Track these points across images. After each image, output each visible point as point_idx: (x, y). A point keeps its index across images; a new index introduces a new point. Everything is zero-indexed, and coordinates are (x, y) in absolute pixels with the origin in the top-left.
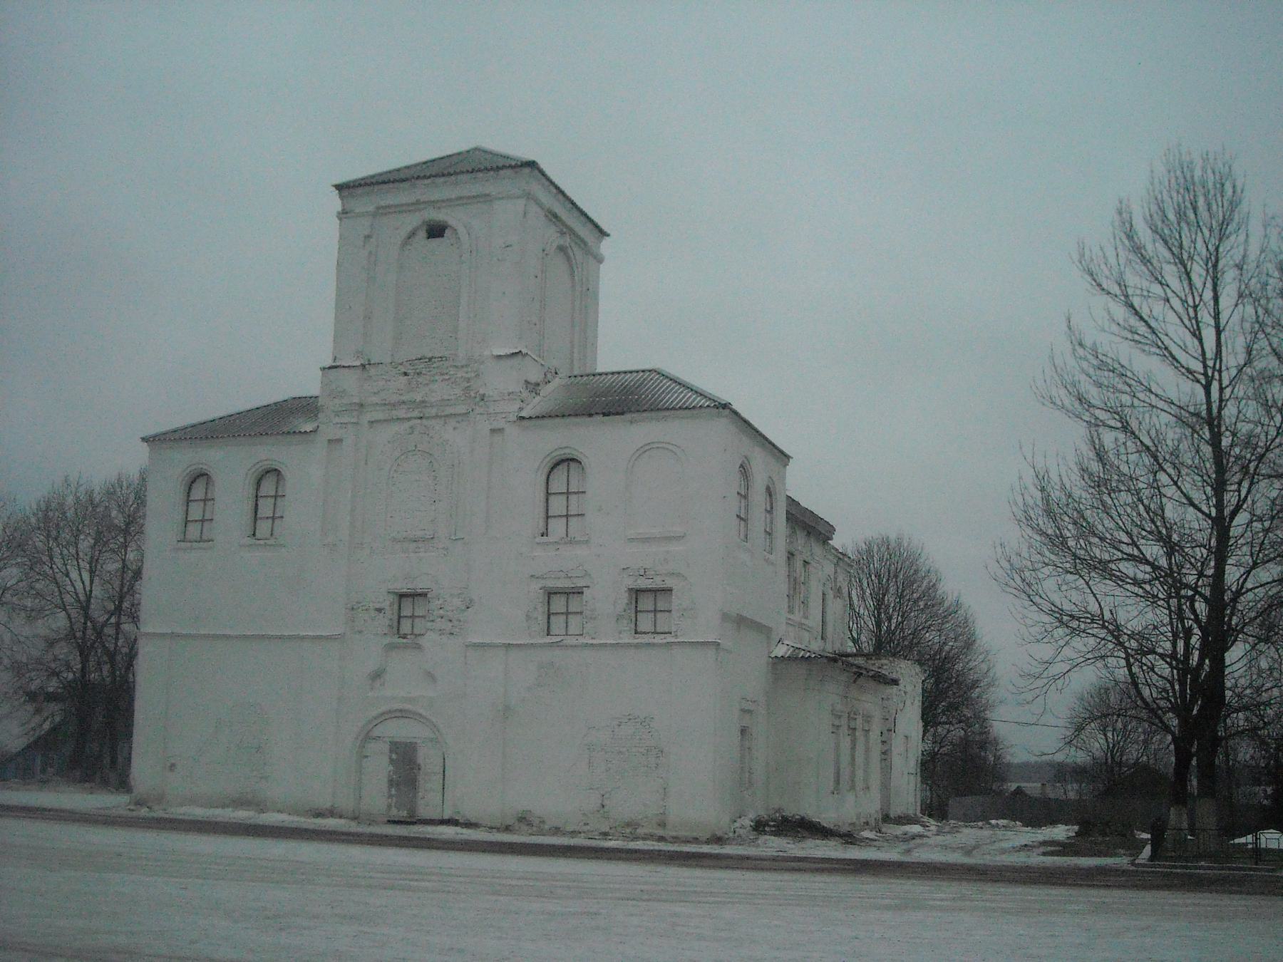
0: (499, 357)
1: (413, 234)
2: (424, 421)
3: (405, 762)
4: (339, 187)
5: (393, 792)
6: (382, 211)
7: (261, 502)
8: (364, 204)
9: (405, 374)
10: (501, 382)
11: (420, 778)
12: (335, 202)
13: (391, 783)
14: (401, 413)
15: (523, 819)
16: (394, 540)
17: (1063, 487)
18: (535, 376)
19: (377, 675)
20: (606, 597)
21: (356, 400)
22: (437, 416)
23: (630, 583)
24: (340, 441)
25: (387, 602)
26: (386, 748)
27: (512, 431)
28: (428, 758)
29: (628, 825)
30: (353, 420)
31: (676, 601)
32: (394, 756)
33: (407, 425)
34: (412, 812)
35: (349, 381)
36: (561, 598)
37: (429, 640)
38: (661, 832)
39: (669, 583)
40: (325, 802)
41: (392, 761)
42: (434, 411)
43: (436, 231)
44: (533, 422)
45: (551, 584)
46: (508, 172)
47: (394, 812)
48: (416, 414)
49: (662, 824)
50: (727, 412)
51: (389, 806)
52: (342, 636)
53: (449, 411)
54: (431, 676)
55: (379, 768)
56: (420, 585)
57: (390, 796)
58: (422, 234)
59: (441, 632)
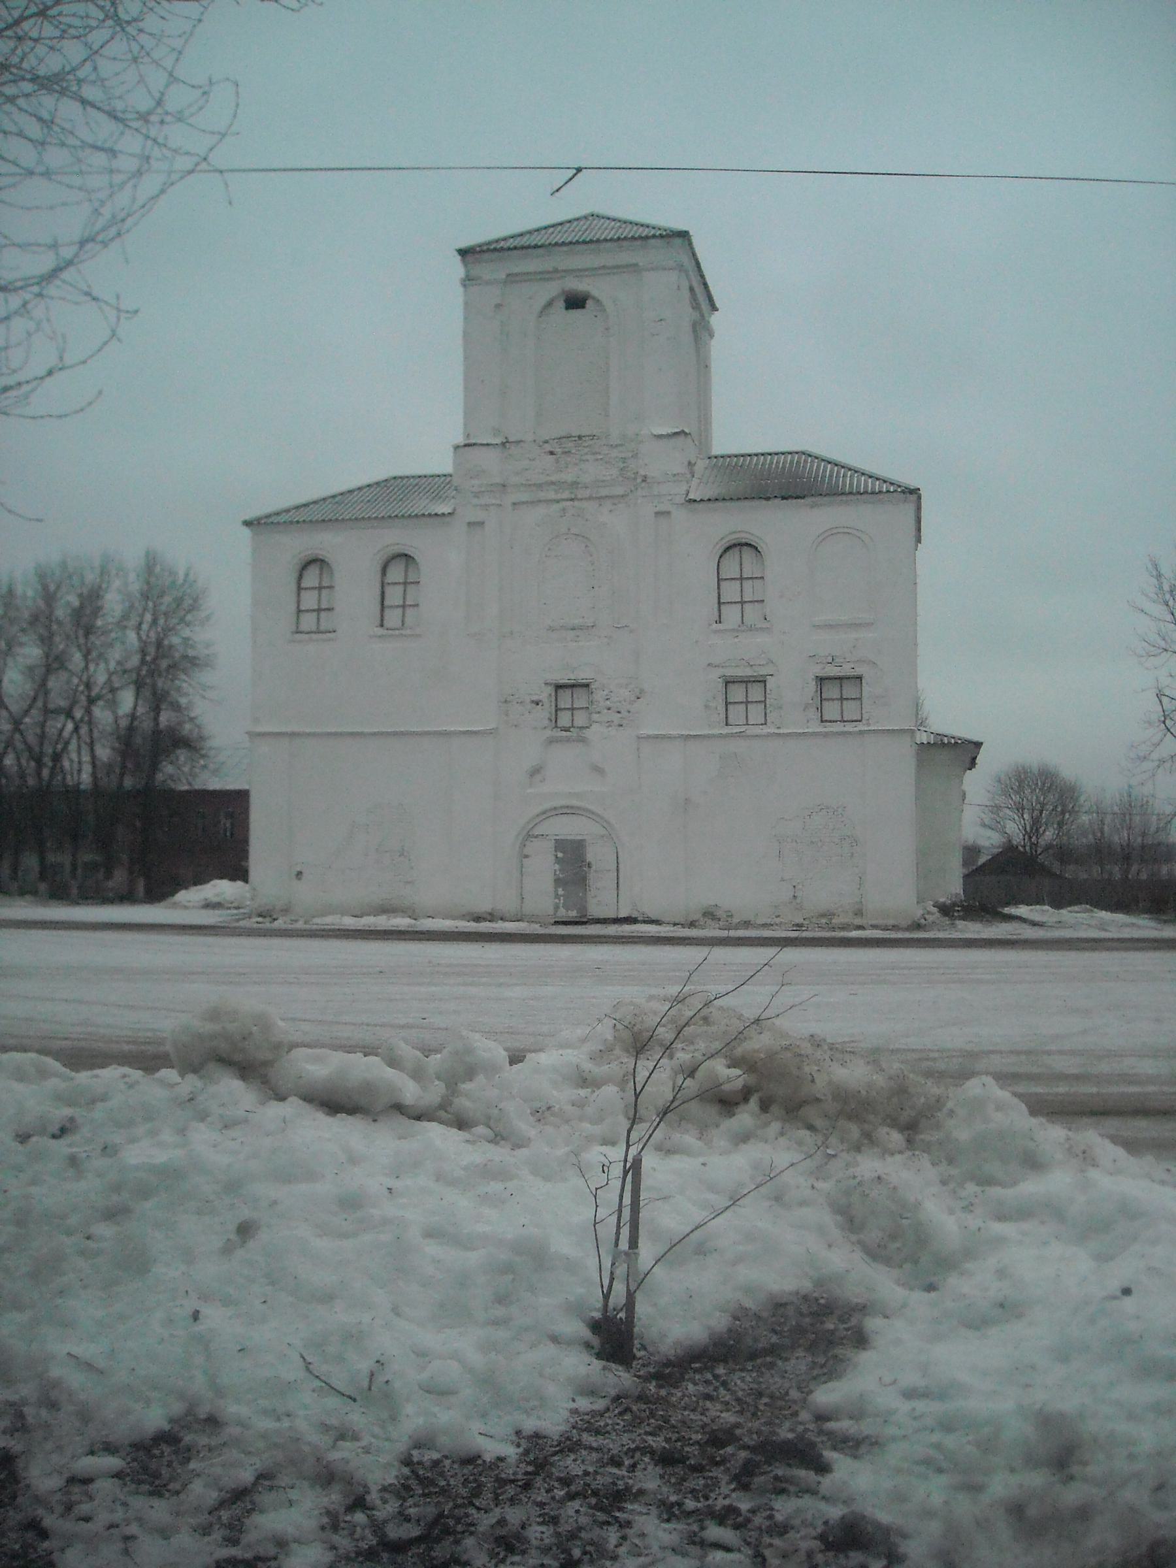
0: (660, 437)
1: (549, 304)
2: (576, 503)
4: (463, 253)
7: (389, 590)
9: (552, 453)
11: (592, 876)
12: (457, 269)
13: (558, 882)
15: (710, 914)
16: (551, 629)
19: (535, 771)
20: (792, 684)
21: (498, 480)
22: (590, 498)
23: (819, 671)
24: (481, 524)
30: (498, 502)
32: (560, 855)
33: (556, 507)
34: (583, 909)
35: (489, 460)
36: (744, 687)
42: (587, 493)
43: (576, 302)
45: (730, 672)
48: (566, 495)
49: (859, 913)
51: (557, 907)
52: (490, 732)
53: (604, 492)
54: (598, 770)
55: (543, 867)
56: (582, 676)
57: (557, 896)
58: (561, 304)
59: (609, 723)
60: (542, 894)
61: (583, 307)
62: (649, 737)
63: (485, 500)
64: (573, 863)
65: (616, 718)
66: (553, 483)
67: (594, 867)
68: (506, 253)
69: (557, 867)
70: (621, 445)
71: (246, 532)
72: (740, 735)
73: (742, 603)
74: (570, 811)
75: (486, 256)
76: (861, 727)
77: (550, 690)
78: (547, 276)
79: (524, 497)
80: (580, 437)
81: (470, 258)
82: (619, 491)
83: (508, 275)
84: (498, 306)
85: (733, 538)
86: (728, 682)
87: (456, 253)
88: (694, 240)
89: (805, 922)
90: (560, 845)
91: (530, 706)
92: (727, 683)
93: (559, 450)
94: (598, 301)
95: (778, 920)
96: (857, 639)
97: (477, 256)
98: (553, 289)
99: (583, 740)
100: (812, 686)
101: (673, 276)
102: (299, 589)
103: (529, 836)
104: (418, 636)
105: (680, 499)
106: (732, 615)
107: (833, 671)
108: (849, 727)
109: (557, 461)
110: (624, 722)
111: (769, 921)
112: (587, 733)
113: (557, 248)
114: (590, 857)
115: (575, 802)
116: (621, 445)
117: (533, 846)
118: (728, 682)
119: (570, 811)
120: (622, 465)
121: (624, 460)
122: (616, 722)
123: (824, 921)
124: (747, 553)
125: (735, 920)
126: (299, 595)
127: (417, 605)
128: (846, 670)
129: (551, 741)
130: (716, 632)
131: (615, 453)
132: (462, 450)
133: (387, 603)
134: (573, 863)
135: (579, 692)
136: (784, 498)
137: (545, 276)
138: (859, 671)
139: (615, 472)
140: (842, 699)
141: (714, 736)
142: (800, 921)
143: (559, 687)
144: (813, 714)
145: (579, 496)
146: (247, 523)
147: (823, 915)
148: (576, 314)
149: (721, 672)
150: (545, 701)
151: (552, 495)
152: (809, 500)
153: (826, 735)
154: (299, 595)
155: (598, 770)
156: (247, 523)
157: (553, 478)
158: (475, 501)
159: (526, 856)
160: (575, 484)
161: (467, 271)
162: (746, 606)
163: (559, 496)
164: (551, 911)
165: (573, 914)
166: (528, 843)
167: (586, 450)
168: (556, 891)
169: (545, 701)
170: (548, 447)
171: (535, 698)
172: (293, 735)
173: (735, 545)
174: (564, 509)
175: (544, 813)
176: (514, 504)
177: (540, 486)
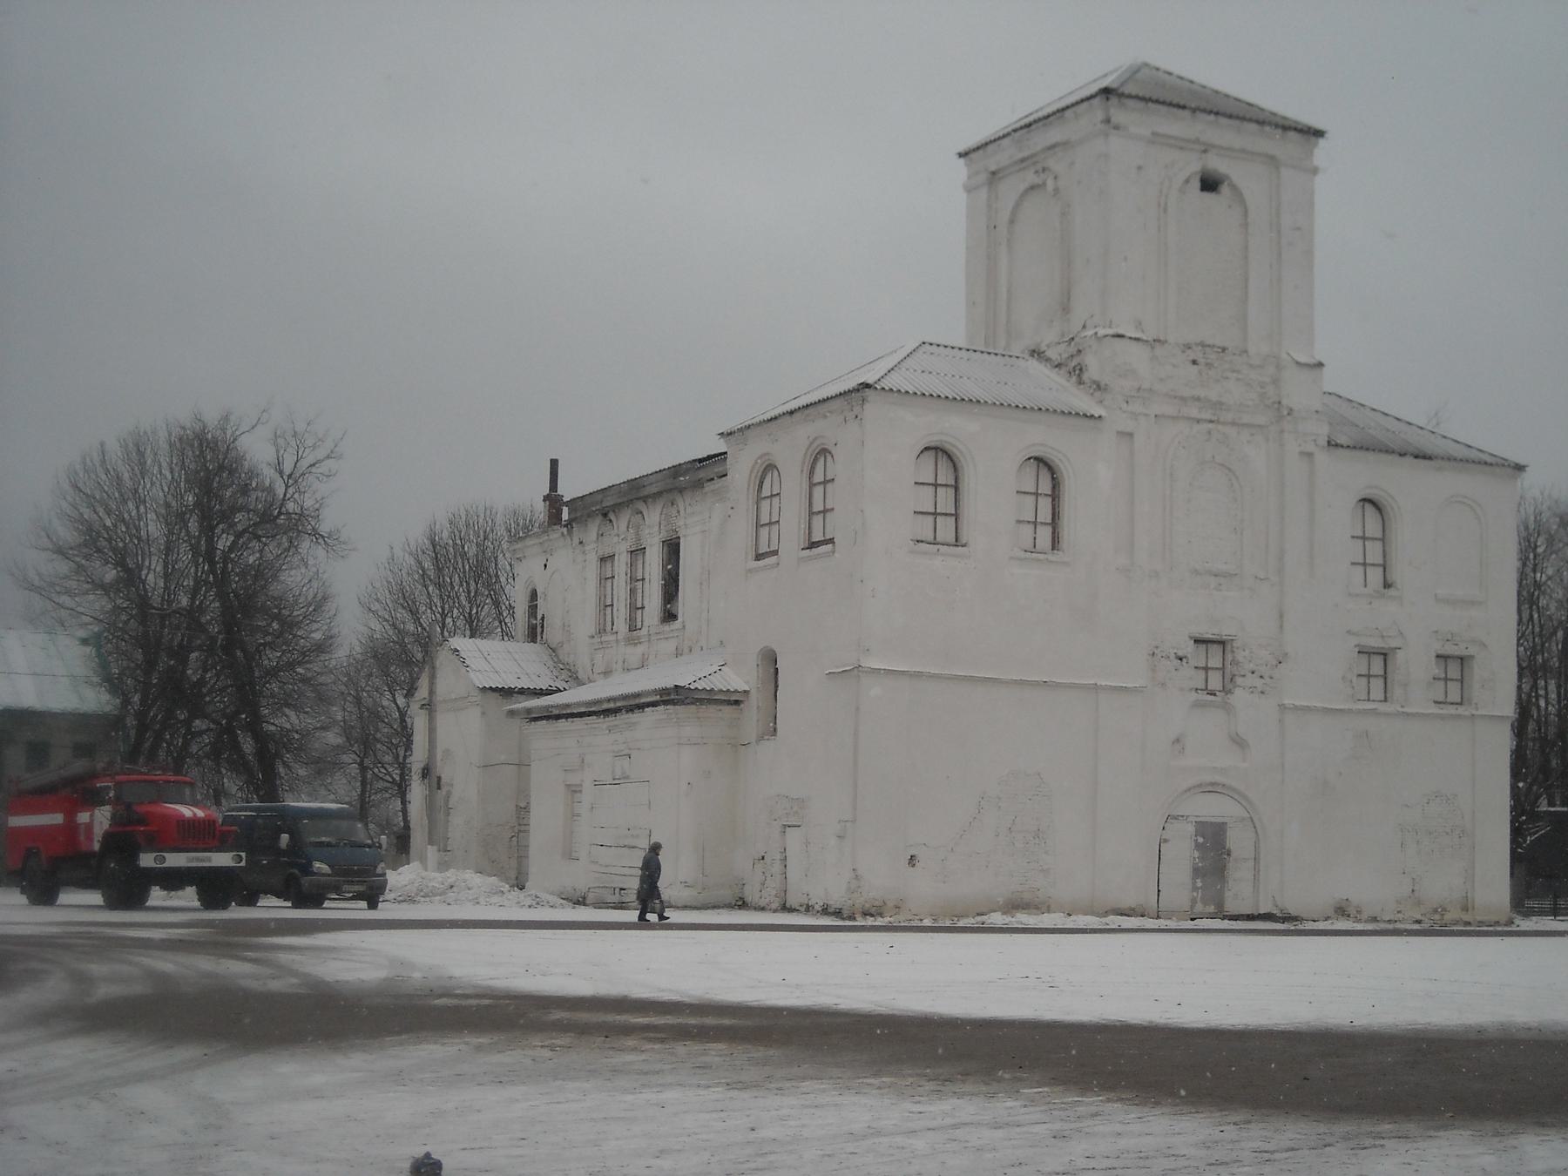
1: (1187, 181)
3: (1213, 840)
5: (1199, 884)
9: (1194, 362)
11: (1231, 865)
13: (1196, 872)
16: (1196, 572)
17: (39, 575)
20: (1416, 664)
22: (1233, 424)
23: (1438, 647)
26: (1191, 829)
27: (1323, 458)
28: (1238, 841)
29: (1435, 911)
32: (1201, 840)
34: (1220, 905)
38: (1466, 918)
39: (1472, 651)
40: (1128, 901)
41: (1198, 846)
42: (1229, 417)
43: (1210, 184)
44: (1347, 452)
46: (1253, 127)
47: (1199, 907)
48: (1208, 416)
50: (874, 408)
51: (1194, 901)
53: (1246, 419)
54: (1239, 742)
55: (1182, 853)
56: (1225, 631)
57: (1195, 889)
58: (1197, 184)
59: (1252, 689)
62: (1296, 708)
64: (1213, 846)
65: (1259, 683)
66: (1198, 399)
69: (1196, 854)
72: (1374, 712)
75: (1131, 103)
79: (1169, 409)
80: (1224, 350)
93: (1201, 360)
94: (1234, 187)
95: (1400, 916)
104: (1065, 563)
109: (1200, 373)
115: (1218, 779)
123: (1437, 917)
127: (1019, 522)
137: (1181, 144)
141: (1350, 711)
142: (1419, 917)
148: (1207, 196)
151: (1194, 413)
153: (1442, 717)
155: (1239, 742)
160: (1219, 405)
162: (1031, 527)
168: (1194, 883)
171: (1180, 654)
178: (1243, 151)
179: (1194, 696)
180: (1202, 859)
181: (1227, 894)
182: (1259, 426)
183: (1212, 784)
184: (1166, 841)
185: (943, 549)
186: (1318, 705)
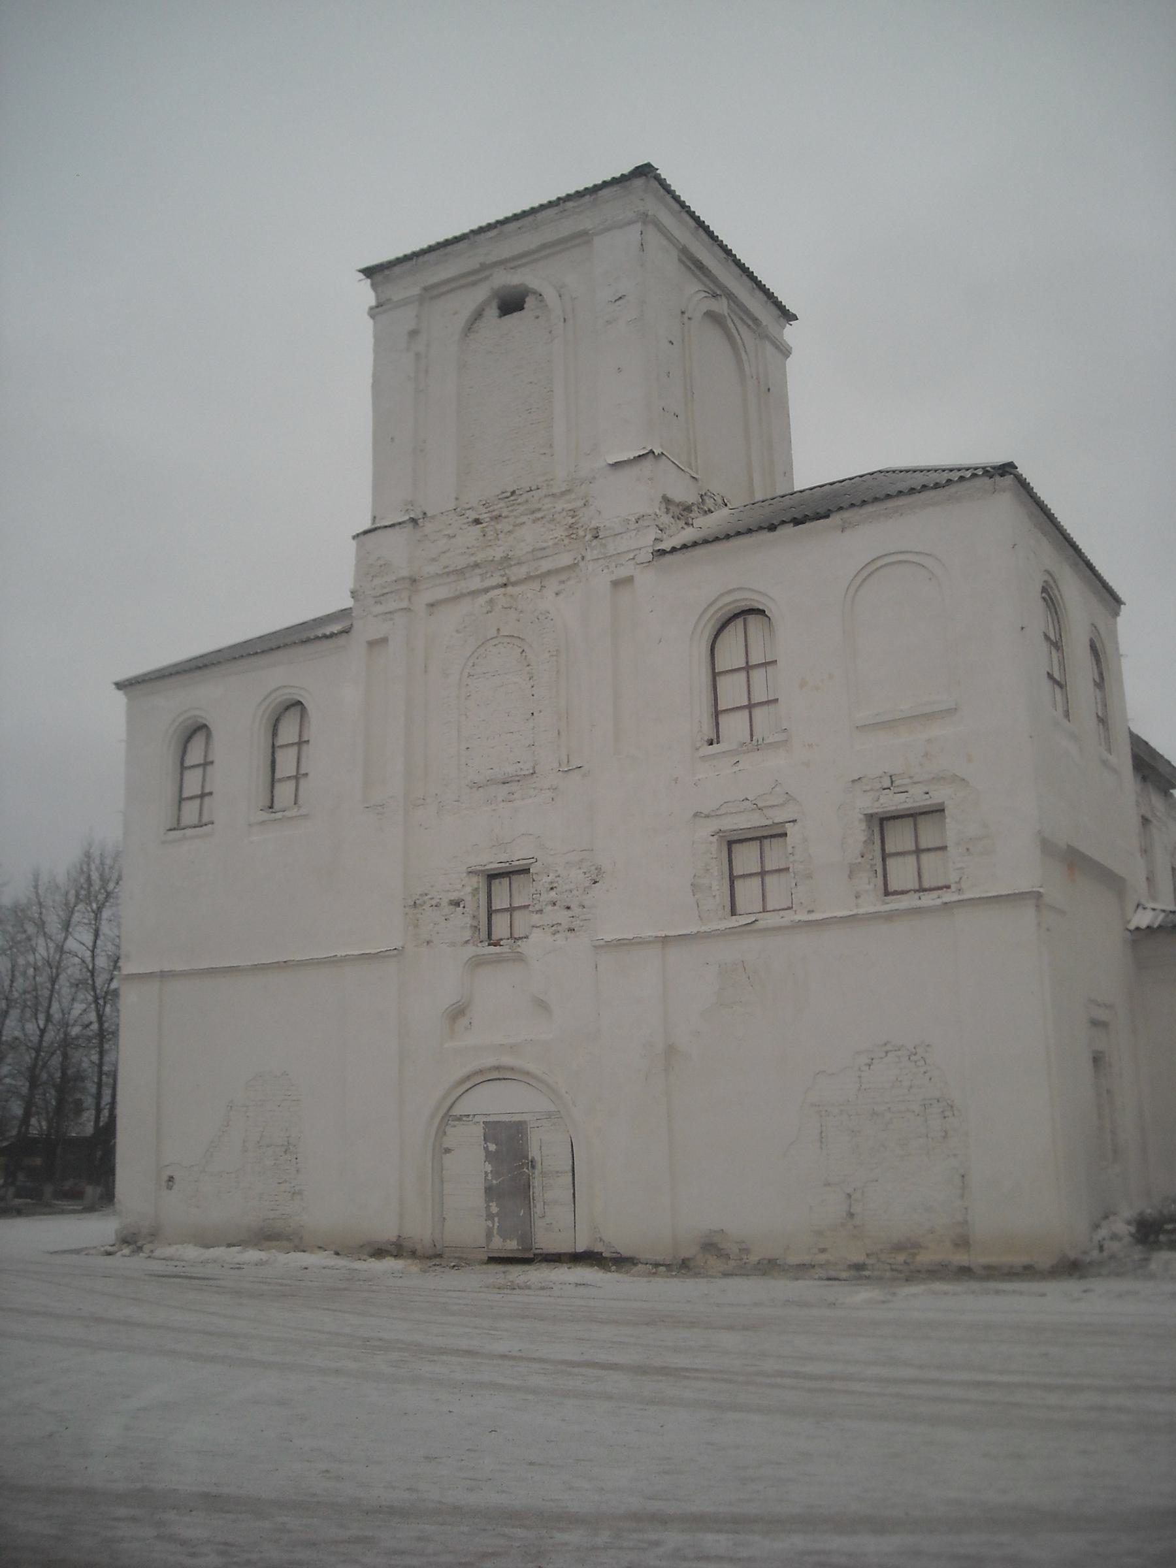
0: (616, 465)
1: (478, 315)
2: (510, 589)
3: (509, 1148)
5: (494, 1209)
6: (431, 293)
7: (280, 756)
8: (407, 288)
9: (477, 522)
10: (625, 502)
12: (366, 294)
13: (489, 1190)
14: (475, 583)
18: (683, 493)
19: (458, 1013)
20: (827, 835)
21: (405, 573)
22: (529, 578)
23: (868, 803)
24: (384, 640)
25: (467, 887)
26: (479, 1131)
27: (646, 579)
28: (546, 1146)
30: (404, 604)
31: (952, 829)
33: (483, 599)
34: (526, 1239)
36: (750, 846)
37: (536, 944)
38: (961, 1258)
41: (489, 1156)
43: (511, 303)
48: (497, 579)
49: (963, 1242)
51: (489, 1235)
52: (398, 952)
53: (546, 565)
55: (470, 1166)
56: (518, 854)
57: (490, 1217)
58: (492, 312)
59: (555, 928)
60: (468, 1217)
61: (521, 308)
63: (392, 605)
64: (512, 1160)
65: (562, 917)
66: (477, 565)
67: (539, 1166)
68: (421, 259)
69: (489, 1168)
70: (569, 491)
71: (120, 697)
73: (750, 707)
74: (500, 1075)
76: (948, 897)
77: (479, 882)
78: (473, 278)
79: (441, 593)
81: (379, 277)
82: (566, 559)
83: (426, 289)
84: (414, 333)
85: (744, 605)
86: (731, 843)
87: (361, 276)
88: (663, 173)
89: (869, 1261)
90: (493, 1130)
91: (447, 909)
92: (730, 843)
93: (485, 517)
94: (535, 292)
95: (822, 1258)
96: (929, 741)
97: (387, 272)
98: (481, 293)
99: (520, 958)
100: (859, 833)
101: (633, 234)
102: (183, 768)
103: (450, 1117)
104: (305, 817)
105: (645, 555)
106: (734, 727)
107: (891, 802)
108: (928, 900)
110: (576, 923)
111: (806, 1259)
112: (523, 946)
113: (483, 236)
114: (534, 1152)
115: (507, 1060)
116: (569, 491)
117: (457, 1134)
118: (731, 843)
119: (500, 1075)
120: (571, 521)
121: (573, 513)
122: (565, 926)
123: (901, 1258)
124: (752, 619)
125: (754, 1259)
126: (182, 774)
128: (915, 799)
129: (477, 963)
130: (703, 758)
131: (561, 505)
132: (362, 537)
133: (278, 775)
134: (512, 1160)
135: (518, 880)
136: (797, 522)
138: (939, 795)
139: (560, 532)
140: (918, 851)
143: (492, 877)
144: (867, 883)
145: (513, 579)
146: (119, 686)
147: (898, 1248)
149: (713, 825)
150: (468, 898)
152: (836, 519)
153: (889, 917)
154: (182, 774)
156: (119, 686)
157: (479, 558)
158: (379, 609)
159: (448, 1151)
161: (377, 297)
163: (489, 583)
164: (482, 1241)
165: (512, 1245)
166: (449, 1130)
167: (521, 509)
168: (488, 1207)
169: (468, 898)
170: (473, 515)
171: (454, 896)
172: (164, 976)
173: (736, 616)
174: (491, 601)
175: (468, 1078)
176: (432, 605)
177: (460, 572)
178: (545, 246)
179: (471, 950)
180: (496, 1173)
181: (539, 1224)
182: (569, 567)
183: (497, 1068)
184: (448, 1151)
185: (189, 832)
186: (356, 953)
